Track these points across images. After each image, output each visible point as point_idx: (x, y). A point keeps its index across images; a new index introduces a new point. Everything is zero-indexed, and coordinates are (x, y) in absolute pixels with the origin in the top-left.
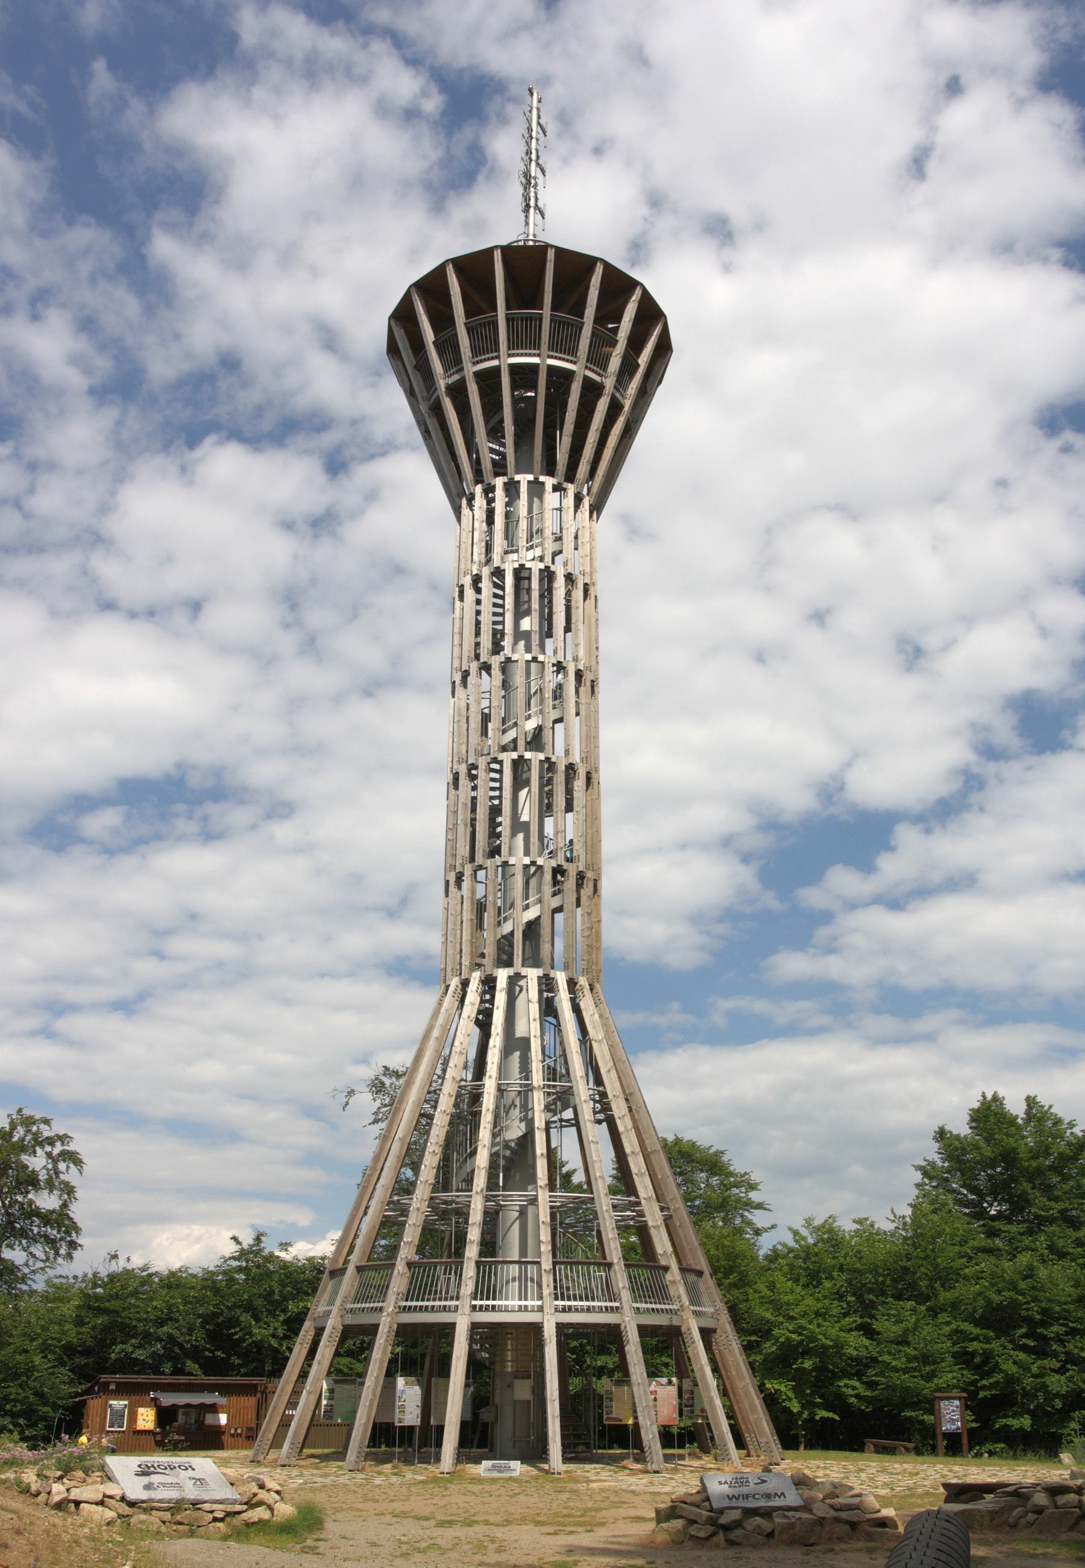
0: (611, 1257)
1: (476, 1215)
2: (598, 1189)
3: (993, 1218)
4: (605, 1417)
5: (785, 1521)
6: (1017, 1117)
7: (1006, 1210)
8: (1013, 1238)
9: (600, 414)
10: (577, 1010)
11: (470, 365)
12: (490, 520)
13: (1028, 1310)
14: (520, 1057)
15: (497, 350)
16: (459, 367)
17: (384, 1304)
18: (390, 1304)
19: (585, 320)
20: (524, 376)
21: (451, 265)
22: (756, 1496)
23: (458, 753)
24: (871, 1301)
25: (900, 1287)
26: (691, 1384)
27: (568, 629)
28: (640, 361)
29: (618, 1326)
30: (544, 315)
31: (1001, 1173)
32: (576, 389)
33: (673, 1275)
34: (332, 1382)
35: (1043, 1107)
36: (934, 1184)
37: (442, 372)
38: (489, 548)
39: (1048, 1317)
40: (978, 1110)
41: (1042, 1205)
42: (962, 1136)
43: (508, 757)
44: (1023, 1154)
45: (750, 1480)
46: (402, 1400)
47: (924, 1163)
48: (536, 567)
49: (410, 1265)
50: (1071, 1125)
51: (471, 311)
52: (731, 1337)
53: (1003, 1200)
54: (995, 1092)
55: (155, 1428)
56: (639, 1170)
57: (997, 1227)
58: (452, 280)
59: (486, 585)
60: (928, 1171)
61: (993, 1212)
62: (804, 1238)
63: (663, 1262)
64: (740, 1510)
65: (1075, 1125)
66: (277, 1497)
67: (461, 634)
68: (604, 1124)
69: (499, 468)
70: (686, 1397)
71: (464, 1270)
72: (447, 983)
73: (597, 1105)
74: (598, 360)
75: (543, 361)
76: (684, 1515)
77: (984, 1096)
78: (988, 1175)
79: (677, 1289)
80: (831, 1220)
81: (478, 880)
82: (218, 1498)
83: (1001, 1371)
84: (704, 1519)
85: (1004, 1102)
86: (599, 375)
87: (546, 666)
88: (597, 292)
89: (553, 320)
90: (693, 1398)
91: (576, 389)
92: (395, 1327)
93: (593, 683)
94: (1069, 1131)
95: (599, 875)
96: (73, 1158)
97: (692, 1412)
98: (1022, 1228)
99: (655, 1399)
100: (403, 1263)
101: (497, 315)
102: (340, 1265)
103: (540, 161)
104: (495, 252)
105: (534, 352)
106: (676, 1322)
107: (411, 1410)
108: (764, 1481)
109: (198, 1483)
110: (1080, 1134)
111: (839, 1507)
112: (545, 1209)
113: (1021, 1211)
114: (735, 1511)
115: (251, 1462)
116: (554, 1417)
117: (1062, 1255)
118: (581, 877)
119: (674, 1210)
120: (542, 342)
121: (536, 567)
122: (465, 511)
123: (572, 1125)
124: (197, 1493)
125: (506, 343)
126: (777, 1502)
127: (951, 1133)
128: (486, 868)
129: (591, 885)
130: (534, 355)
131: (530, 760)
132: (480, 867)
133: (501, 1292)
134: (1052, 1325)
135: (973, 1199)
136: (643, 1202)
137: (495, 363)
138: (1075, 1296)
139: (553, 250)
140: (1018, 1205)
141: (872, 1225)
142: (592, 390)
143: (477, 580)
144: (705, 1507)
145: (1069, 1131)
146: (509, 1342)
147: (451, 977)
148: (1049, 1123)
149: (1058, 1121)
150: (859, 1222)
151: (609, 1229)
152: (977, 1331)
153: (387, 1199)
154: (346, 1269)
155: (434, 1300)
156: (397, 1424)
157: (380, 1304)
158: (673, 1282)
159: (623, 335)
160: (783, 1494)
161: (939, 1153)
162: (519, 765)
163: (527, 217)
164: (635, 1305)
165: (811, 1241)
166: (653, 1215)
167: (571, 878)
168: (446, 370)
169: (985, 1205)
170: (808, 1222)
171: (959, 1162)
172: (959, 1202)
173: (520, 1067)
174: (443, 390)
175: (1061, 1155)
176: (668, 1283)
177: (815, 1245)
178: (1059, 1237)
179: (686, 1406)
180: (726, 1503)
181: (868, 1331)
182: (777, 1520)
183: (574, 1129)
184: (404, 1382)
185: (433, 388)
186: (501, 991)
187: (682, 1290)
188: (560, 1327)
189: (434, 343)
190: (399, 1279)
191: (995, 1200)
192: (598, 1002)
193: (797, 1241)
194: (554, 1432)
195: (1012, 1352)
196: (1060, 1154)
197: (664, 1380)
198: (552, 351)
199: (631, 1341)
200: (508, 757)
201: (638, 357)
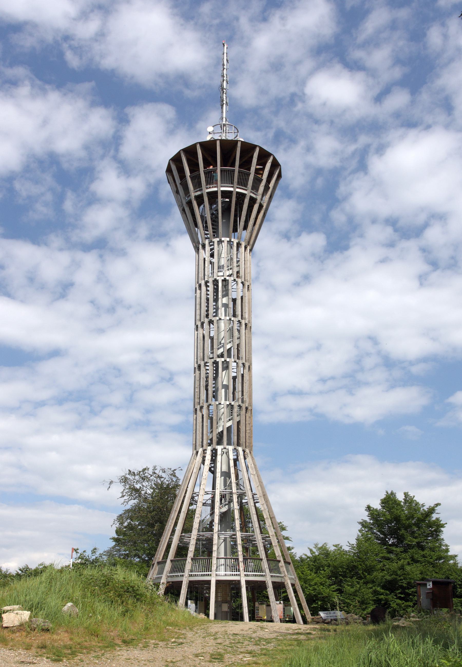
0: (262, 557)
2: (256, 531)
3: (390, 545)
4: (256, 616)
6: (401, 501)
7: (396, 542)
8: (398, 554)
9: (255, 212)
11: (205, 189)
13: (402, 583)
14: (224, 479)
15: (217, 183)
16: (200, 189)
17: (183, 574)
18: (186, 573)
19: (251, 172)
20: (226, 194)
21: (199, 145)
23: (200, 356)
24: (341, 579)
25: (352, 573)
28: (270, 186)
29: (265, 581)
30: (236, 170)
31: (394, 526)
35: (411, 497)
36: (366, 530)
37: (193, 189)
39: (410, 585)
40: (385, 499)
41: (409, 540)
42: (378, 509)
44: (403, 517)
47: (362, 521)
49: (171, 561)
50: (423, 505)
51: (206, 164)
53: (395, 538)
54: (392, 491)
56: (269, 525)
57: (392, 549)
58: (199, 151)
60: (364, 524)
61: (390, 543)
62: (314, 553)
63: (278, 559)
65: (424, 506)
71: (213, 561)
75: (235, 190)
77: (387, 492)
78: (388, 526)
80: (325, 545)
83: (392, 607)
85: (396, 495)
87: (235, 322)
88: (256, 160)
89: (239, 172)
92: (188, 582)
94: (422, 508)
98: (402, 549)
100: (190, 559)
101: (217, 169)
104: (217, 141)
105: (231, 185)
106: (283, 581)
110: (426, 510)
112: (239, 538)
113: (402, 542)
117: (417, 562)
118: (247, 408)
119: (280, 540)
120: (234, 182)
122: (201, 251)
127: (373, 508)
129: (250, 411)
130: (231, 187)
134: (411, 589)
135: (382, 537)
136: (271, 536)
137: (215, 189)
138: (421, 578)
140: (400, 539)
141: (341, 547)
145: (422, 508)
147: (198, 448)
148: (414, 505)
149: (417, 504)
150: (336, 546)
151: (261, 546)
152: (382, 591)
153: (180, 535)
157: (182, 574)
158: (282, 566)
159: (265, 177)
161: (368, 516)
165: (317, 554)
166: (275, 541)
167: (243, 410)
168: (194, 189)
169: (387, 539)
170: (316, 545)
171: (377, 520)
172: (377, 538)
173: (224, 485)
174: (193, 197)
177: (318, 555)
178: (416, 554)
186: (219, 455)
187: (285, 569)
188: (247, 582)
189: (190, 176)
190: (168, 565)
191: (392, 538)
193: (311, 554)
194: (246, 618)
195: (396, 600)
196: (418, 518)
199: (270, 587)
200: (220, 360)
201: (269, 184)
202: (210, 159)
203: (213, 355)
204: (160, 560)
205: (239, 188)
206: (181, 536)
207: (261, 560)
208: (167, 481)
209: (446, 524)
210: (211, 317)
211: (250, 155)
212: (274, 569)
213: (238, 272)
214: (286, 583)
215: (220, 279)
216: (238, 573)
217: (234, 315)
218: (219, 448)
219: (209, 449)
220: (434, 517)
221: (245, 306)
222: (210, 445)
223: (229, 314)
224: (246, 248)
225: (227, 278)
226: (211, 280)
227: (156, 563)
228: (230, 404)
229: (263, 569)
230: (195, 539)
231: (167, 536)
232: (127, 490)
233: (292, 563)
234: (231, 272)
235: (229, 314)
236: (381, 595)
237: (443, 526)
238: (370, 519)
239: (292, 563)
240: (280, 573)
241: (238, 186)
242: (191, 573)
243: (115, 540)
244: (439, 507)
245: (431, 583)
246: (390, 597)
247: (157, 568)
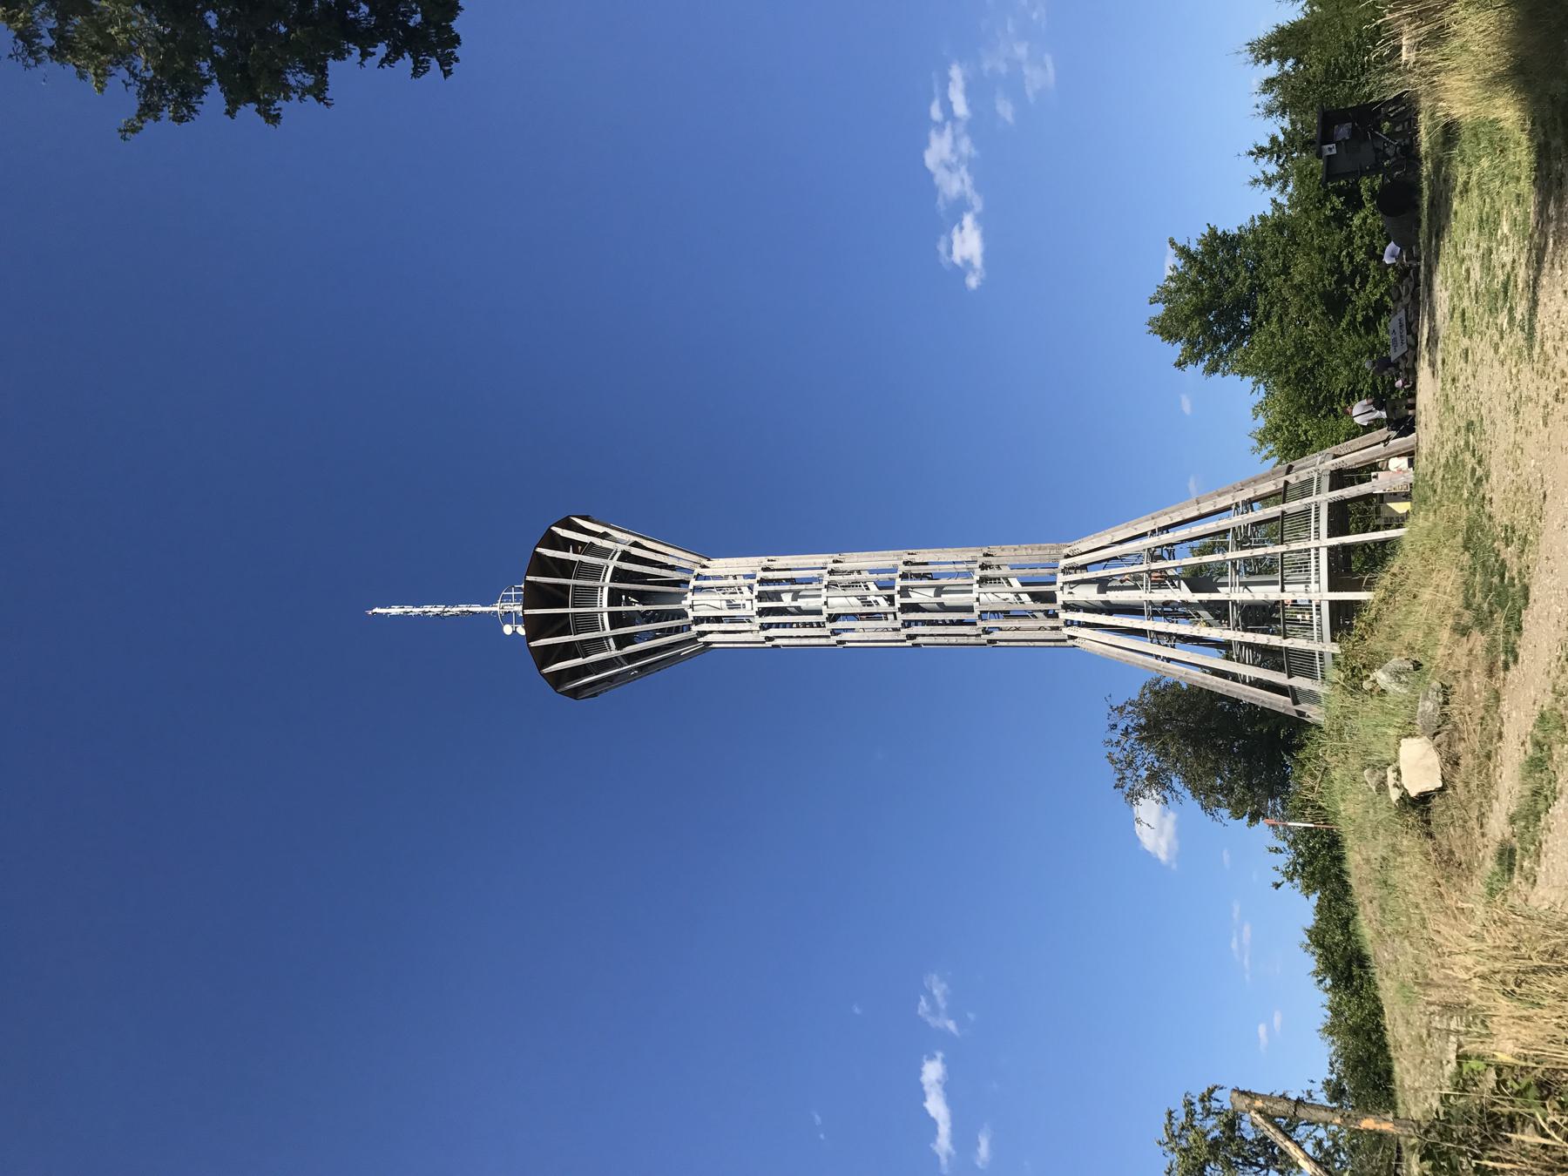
0: (1277, 512)
20: (615, 597)
28: (601, 532)
29: (1329, 504)
32: (626, 566)
33: (1290, 478)
48: (757, 588)
49: (1290, 676)
51: (565, 631)
60: (1212, 369)
63: (1281, 485)
65: (1175, 266)
72: (1067, 638)
74: (605, 553)
79: (1303, 474)
91: (626, 566)
96: (1208, 1096)
106: (1328, 473)
120: (593, 585)
121: (757, 588)
136: (1236, 501)
137: (606, 616)
145: (1180, 269)
152: (1347, 318)
153: (1236, 663)
157: (1317, 656)
158: (1297, 478)
161: (1197, 364)
168: (606, 650)
175: (1200, 272)
176: (1298, 481)
190: (1299, 682)
200: (898, 600)
202: (559, 626)
203: (890, 613)
204: (1289, 699)
205: (604, 578)
206: (1238, 661)
207: (1283, 512)
208: (1132, 721)
209: (1209, 225)
210: (822, 618)
211: (551, 564)
212: (1305, 489)
213: (746, 577)
214: (1333, 469)
215: (758, 605)
216: (1313, 552)
217: (819, 580)
218: (1062, 597)
219: (1064, 615)
220: (1194, 247)
221: (803, 564)
222: (1055, 616)
223: (818, 589)
224: (704, 567)
225: (756, 593)
226: (758, 620)
227: (1296, 707)
229: (1303, 508)
230: (1243, 633)
231: (1240, 688)
232: (1154, 791)
234: (745, 589)
235: (818, 589)
236: (1355, 319)
237: (1213, 232)
238: (1203, 360)
240: (1312, 479)
241: (602, 579)
242: (1316, 638)
243: (1255, 817)
244: (1176, 241)
245: (1326, 147)
246: (1360, 303)
247: (1303, 705)
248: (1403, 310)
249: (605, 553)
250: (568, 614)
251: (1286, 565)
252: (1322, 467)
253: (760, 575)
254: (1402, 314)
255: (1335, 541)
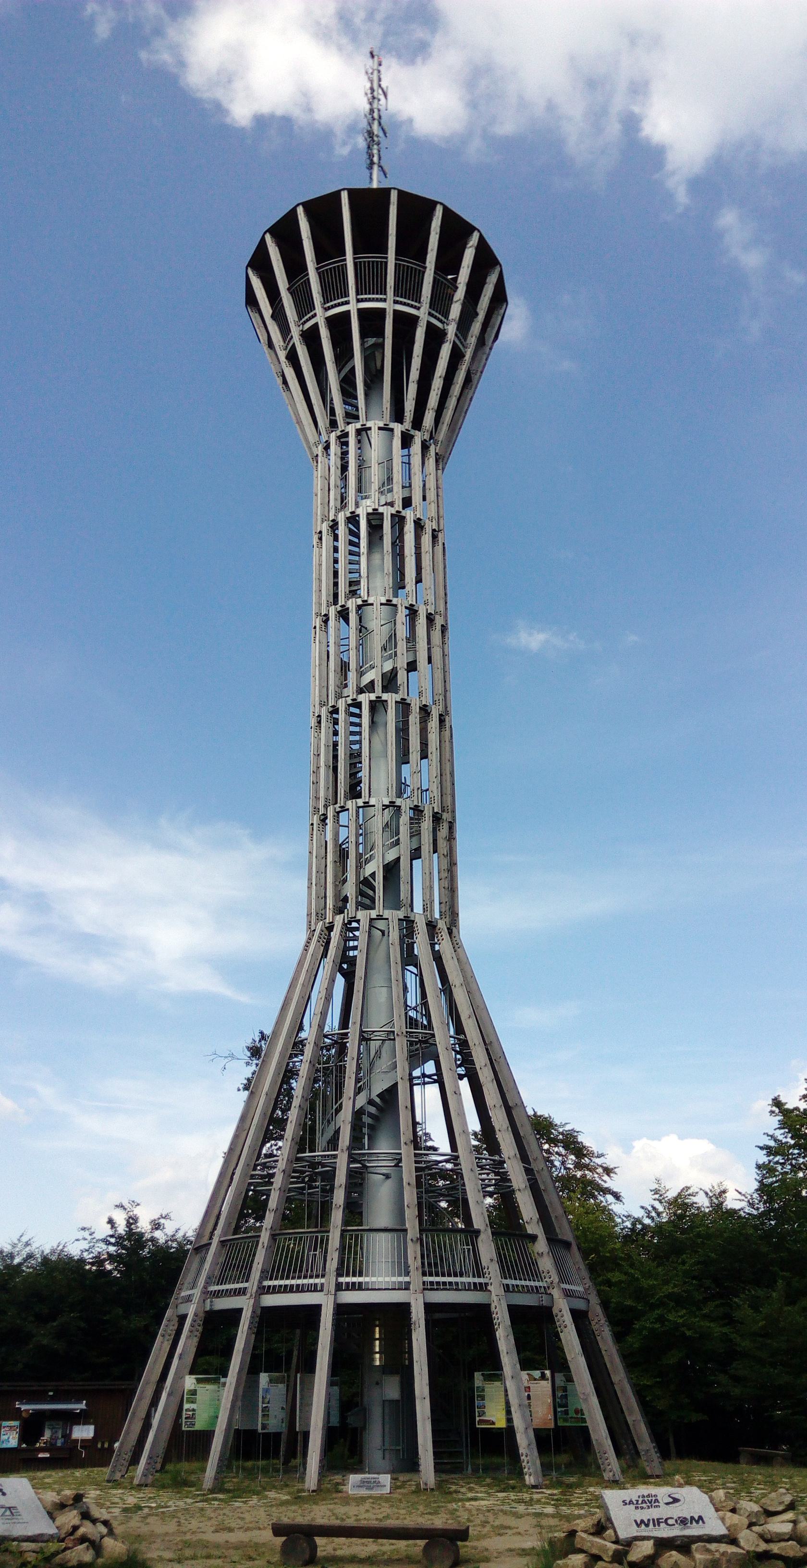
1: (341, 1178)
4: (477, 1419)
5: (709, 1557)
10: (438, 958)
12: (344, 468)
19: (428, 264)
22: (670, 1522)
26: (564, 1379)
27: (419, 580)
28: (478, 310)
34: (195, 1381)
38: (343, 498)
43: (365, 699)
45: (659, 1498)
46: (267, 1400)
48: (387, 511)
51: (320, 256)
52: (603, 1322)
55: (20, 1444)
59: (342, 530)
64: (651, 1542)
66: (104, 1530)
67: (320, 580)
68: (466, 1079)
69: (352, 416)
70: (560, 1394)
73: (459, 1056)
74: (441, 303)
76: (585, 1548)
81: (341, 823)
82: (30, 1534)
84: (611, 1553)
86: (441, 321)
90: (566, 1397)
93: (444, 629)
95: (454, 818)
97: (566, 1412)
99: (529, 1397)
102: (205, 1241)
103: (382, 164)
107: (275, 1413)
108: (676, 1500)
109: (8, 1513)
111: (769, 1537)
114: (646, 1542)
115: (108, 1481)
116: (424, 1420)
121: (387, 511)
123: (435, 1081)
124: (6, 1526)
125: (354, 290)
126: (694, 1531)
128: (348, 810)
131: (386, 701)
132: (344, 809)
133: (367, 1271)
139: (396, 192)
142: (435, 337)
143: (334, 526)
144: (610, 1536)
146: (377, 1329)
154: (210, 1244)
155: (299, 1278)
156: (260, 1430)
158: (541, 1255)
160: (700, 1518)
162: (377, 706)
163: (371, 174)
164: (506, 1282)
179: (560, 1406)
180: (634, 1531)
181: (728, 1319)
182: (698, 1556)
183: (437, 1085)
184: (268, 1379)
185: (289, 337)
192: (457, 946)
197: (537, 1374)
198: (398, 296)
200: (365, 699)
214: (555, 1311)
222: (340, 910)
224: (425, 447)
226: (341, 518)
228: (392, 803)
233: (574, 1248)
239: (574, 1248)
241: (398, 299)
248: (722, 1530)
249: (441, 303)
250: (344, 254)
251: (456, 1238)
252: (556, 1293)
253: (409, 515)
254: (714, 1526)
255: (418, 1314)
